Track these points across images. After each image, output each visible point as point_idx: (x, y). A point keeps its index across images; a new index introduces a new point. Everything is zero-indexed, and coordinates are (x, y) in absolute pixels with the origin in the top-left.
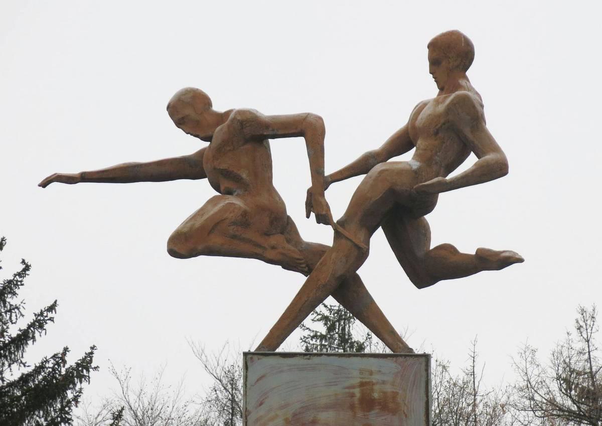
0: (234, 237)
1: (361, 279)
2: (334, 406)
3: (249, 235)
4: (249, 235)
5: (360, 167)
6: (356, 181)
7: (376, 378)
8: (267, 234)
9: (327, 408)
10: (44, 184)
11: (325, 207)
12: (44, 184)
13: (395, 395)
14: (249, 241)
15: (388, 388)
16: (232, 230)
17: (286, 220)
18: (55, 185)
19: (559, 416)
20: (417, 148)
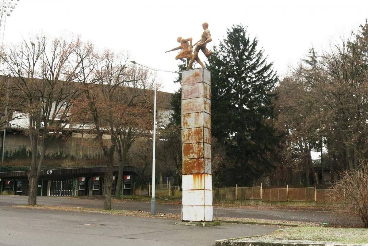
0: (182, 56)
1: (182, 182)
2: (192, 76)
3: (184, 55)
4: (184, 55)
5: (196, 44)
6: (196, 46)
7: (197, 72)
8: (187, 55)
9: (191, 77)
10: (166, 52)
11: (204, 27)
12: (166, 52)
13: (199, 74)
14: (184, 56)
15: (198, 73)
16: (182, 55)
17: (204, 27)
18: (167, 52)
19: (303, 226)
20: (241, 75)
